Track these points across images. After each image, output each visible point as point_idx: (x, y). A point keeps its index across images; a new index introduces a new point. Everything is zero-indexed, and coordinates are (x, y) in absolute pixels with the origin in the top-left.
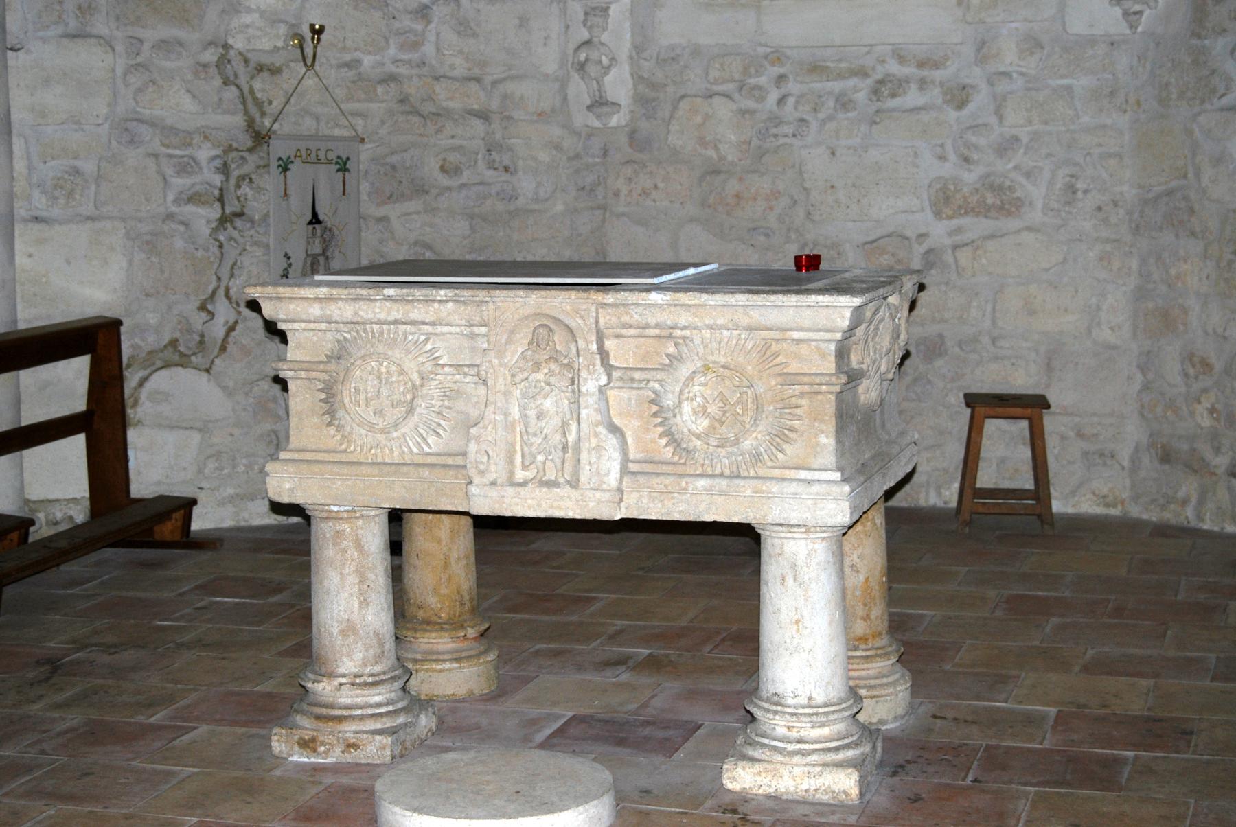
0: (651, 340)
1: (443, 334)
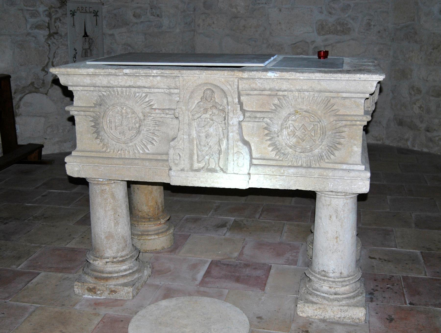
0: (265, 97)
1: (154, 93)
